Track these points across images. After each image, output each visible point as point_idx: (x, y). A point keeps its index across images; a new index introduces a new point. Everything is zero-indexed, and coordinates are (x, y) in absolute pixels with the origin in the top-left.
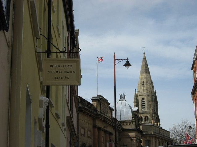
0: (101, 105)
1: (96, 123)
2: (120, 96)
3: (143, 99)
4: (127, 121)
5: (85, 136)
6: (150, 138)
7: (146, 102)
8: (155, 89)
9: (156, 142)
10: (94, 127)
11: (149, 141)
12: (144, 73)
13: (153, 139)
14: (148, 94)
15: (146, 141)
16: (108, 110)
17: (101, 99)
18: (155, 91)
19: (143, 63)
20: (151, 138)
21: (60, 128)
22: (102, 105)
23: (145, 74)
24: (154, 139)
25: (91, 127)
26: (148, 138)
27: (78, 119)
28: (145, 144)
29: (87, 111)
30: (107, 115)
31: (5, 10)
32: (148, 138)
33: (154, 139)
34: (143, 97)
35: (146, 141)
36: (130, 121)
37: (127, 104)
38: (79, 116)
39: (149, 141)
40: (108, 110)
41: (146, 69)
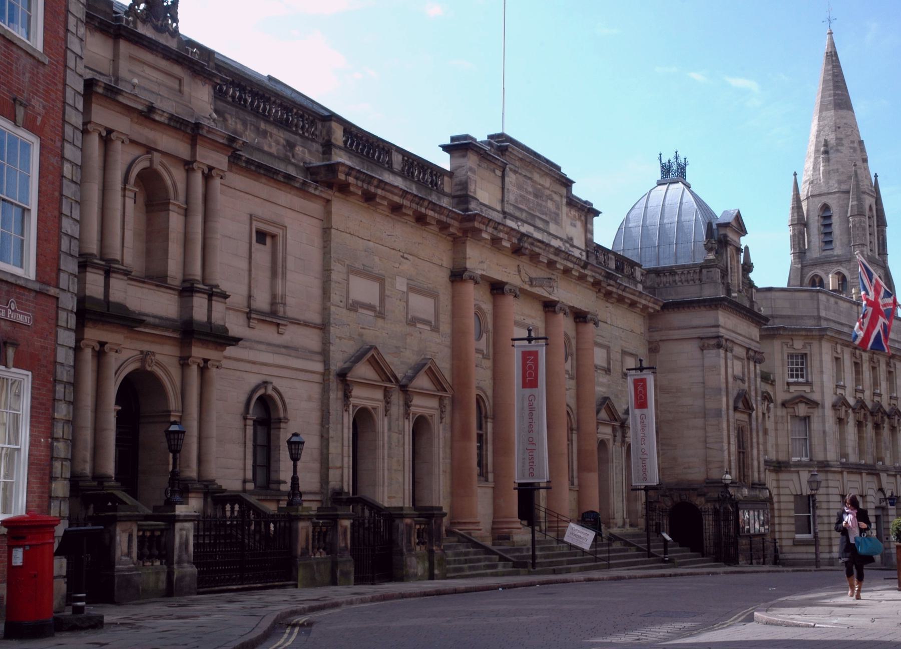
0: (503, 177)
1: (465, 258)
2: (663, 167)
3: (826, 208)
4: (683, 267)
5: (380, 314)
6: (810, 344)
7: (835, 220)
8: (874, 166)
9: (857, 365)
10: (458, 276)
11: (804, 356)
12: (827, 109)
13: (821, 346)
14: (844, 187)
15: (791, 356)
16: (558, 208)
17: (503, 150)
18: (876, 176)
19: (826, 71)
20: (815, 344)
21: (246, 281)
22: (511, 178)
23: (832, 113)
24: (826, 347)
25: (440, 278)
26: (798, 344)
27: (326, 231)
28: (786, 369)
29: (379, 192)
30: (553, 228)
31: (805, 212)
32: (798, 344)
33: (826, 347)
34: (824, 200)
35: (791, 356)
36: (695, 265)
37: (688, 197)
38: (333, 210)
39: (804, 356)
40: (558, 208)
41: (835, 95)
